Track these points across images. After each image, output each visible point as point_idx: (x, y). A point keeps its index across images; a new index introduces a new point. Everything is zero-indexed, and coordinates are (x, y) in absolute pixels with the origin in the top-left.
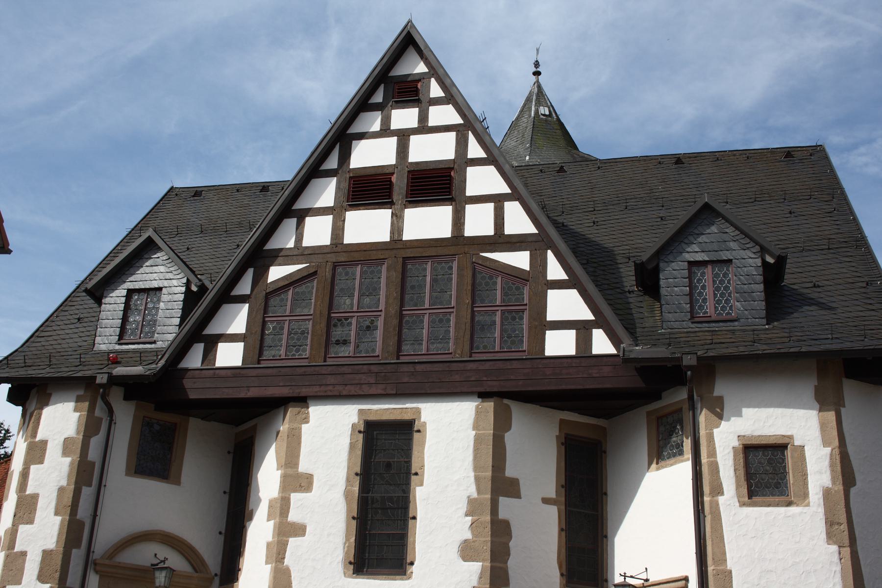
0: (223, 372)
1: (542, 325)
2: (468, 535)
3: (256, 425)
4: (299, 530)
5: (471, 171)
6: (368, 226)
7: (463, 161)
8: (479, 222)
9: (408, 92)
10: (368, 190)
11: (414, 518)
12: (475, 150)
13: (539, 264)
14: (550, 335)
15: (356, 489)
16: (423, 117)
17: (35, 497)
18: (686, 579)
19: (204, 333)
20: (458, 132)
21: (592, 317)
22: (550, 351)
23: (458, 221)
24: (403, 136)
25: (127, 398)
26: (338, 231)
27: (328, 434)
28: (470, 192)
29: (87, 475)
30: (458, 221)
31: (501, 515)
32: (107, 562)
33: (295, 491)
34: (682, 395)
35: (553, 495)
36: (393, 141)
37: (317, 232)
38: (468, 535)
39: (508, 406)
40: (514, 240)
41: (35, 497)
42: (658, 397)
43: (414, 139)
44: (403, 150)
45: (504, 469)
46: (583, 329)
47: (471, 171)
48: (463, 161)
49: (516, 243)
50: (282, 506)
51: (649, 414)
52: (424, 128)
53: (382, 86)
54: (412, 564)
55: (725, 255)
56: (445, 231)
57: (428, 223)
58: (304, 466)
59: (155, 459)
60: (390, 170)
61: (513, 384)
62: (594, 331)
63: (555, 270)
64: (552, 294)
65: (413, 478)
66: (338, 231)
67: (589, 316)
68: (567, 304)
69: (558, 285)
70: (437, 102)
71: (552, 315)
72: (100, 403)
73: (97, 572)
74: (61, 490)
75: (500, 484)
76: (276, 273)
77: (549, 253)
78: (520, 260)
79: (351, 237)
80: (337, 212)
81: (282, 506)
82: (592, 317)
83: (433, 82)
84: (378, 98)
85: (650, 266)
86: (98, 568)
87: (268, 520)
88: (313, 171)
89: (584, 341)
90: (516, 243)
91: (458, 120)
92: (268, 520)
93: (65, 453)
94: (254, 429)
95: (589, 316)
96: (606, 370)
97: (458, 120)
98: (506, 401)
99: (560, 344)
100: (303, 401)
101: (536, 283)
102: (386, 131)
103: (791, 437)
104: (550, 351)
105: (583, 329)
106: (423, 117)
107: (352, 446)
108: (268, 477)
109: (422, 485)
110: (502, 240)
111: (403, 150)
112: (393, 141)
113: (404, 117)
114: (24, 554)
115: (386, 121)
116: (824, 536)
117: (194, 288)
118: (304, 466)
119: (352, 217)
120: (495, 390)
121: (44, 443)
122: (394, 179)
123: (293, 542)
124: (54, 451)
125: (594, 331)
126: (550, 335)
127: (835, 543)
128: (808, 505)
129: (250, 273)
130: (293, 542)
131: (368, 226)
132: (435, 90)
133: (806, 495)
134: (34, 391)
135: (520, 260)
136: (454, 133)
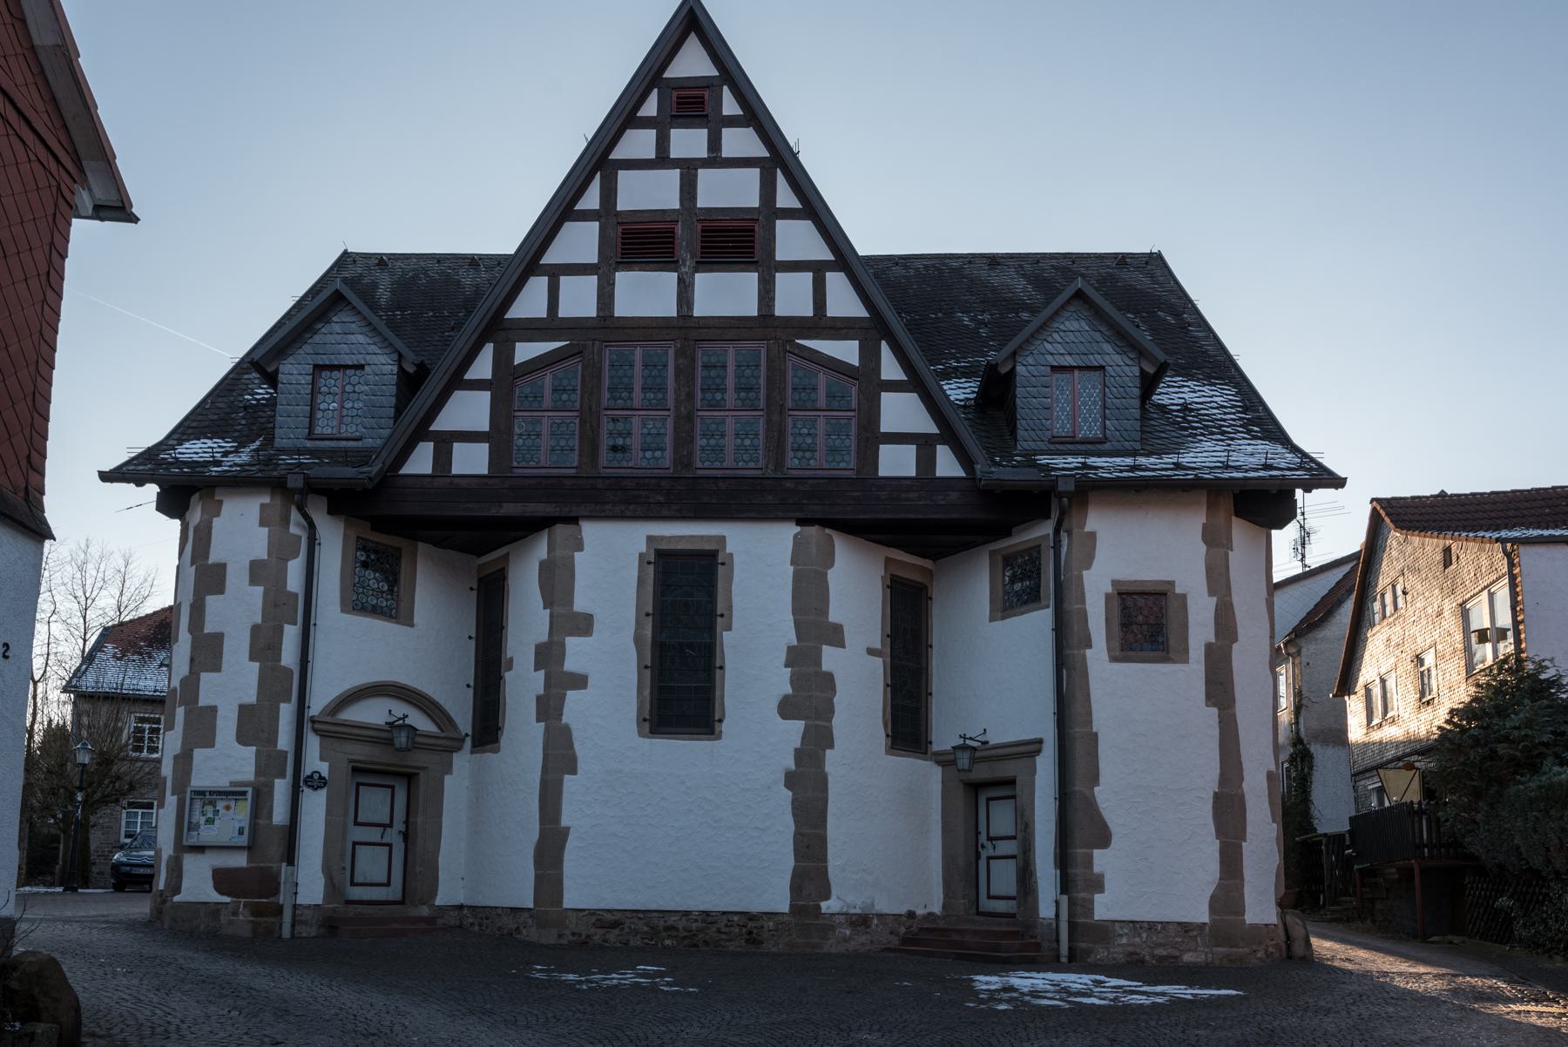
0: (464, 482)
1: (872, 437)
2: (789, 690)
3: (507, 554)
4: (580, 681)
5: (781, 225)
6: (646, 294)
7: (770, 212)
8: (793, 297)
9: (691, 105)
10: (639, 242)
11: (721, 668)
12: (785, 198)
13: (870, 356)
14: (885, 451)
15: (648, 633)
16: (715, 143)
17: (218, 638)
18: (1040, 741)
19: (402, 472)
20: (762, 168)
21: (935, 430)
22: (884, 470)
23: (767, 294)
24: (689, 169)
25: (332, 511)
26: (606, 296)
27: (610, 561)
28: (781, 255)
29: (289, 610)
30: (767, 294)
31: (209, 627)
32: (329, 719)
33: (571, 635)
34: (1045, 529)
35: (878, 646)
36: (675, 175)
37: (579, 299)
38: (789, 690)
39: (830, 537)
40: (839, 324)
41: (218, 638)
42: (1007, 533)
43: (703, 174)
44: (688, 189)
45: (827, 613)
46: (925, 444)
47: (781, 225)
48: (770, 212)
49: (841, 329)
50: (549, 655)
51: (992, 553)
52: (715, 160)
53: (598, 176)
54: (720, 721)
55: (1095, 360)
56: (749, 307)
57: (726, 294)
58: (581, 604)
59: (379, 589)
60: (674, 217)
61: (841, 506)
62: (939, 447)
63: (890, 368)
64: (886, 397)
65: (719, 620)
66: (606, 296)
67: (932, 429)
68: (901, 412)
69: (894, 386)
70: (732, 122)
71: (886, 426)
72: (295, 515)
73: (315, 731)
74: (1095, 779)
75: (814, 627)
76: (525, 351)
77: (883, 343)
78: (847, 351)
79: (625, 306)
80: (603, 271)
81: (549, 655)
82: (935, 430)
83: (727, 93)
84: (650, 108)
85: (1004, 370)
86: (317, 726)
87: (536, 669)
88: (562, 210)
89: (926, 460)
90: (841, 329)
91: (761, 152)
92: (536, 669)
93: (254, 581)
94: (506, 557)
95: (932, 429)
96: (954, 496)
97: (761, 152)
98: (827, 531)
99: (897, 462)
100: (574, 520)
101: (867, 380)
102: (662, 160)
103: (1172, 583)
104: (884, 470)
105: (925, 444)
106: (715, 143)
107: (641, 582)
108: (527, 620)
109: (729, 628)
110: (821, 324)
111: (688, 189)
112: (675, 175)
113: (688, 142)
114: (213, 710)
115: (663, 143)
116: (1203, 696)
117: (411, 369)
118: (581, 604)
119: (624, 280)
120: (819, 516)
121: (222, 567)
122: (679, 229)
123: (572, 696)
124: (237, 578)
125: (939, 447)
126: (885, 451)
127: (1214, 705)
128: (1186, 661)
129: (488, 351)
130: (572, 696)
131: (646, 294)
132: (730, 106)
133: (1186, 650)
134: (195, 498)
135: (847, 351)
136: (454, 471)
